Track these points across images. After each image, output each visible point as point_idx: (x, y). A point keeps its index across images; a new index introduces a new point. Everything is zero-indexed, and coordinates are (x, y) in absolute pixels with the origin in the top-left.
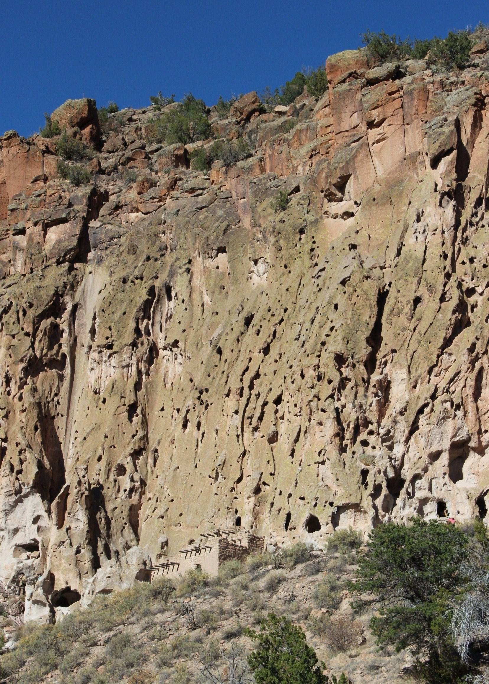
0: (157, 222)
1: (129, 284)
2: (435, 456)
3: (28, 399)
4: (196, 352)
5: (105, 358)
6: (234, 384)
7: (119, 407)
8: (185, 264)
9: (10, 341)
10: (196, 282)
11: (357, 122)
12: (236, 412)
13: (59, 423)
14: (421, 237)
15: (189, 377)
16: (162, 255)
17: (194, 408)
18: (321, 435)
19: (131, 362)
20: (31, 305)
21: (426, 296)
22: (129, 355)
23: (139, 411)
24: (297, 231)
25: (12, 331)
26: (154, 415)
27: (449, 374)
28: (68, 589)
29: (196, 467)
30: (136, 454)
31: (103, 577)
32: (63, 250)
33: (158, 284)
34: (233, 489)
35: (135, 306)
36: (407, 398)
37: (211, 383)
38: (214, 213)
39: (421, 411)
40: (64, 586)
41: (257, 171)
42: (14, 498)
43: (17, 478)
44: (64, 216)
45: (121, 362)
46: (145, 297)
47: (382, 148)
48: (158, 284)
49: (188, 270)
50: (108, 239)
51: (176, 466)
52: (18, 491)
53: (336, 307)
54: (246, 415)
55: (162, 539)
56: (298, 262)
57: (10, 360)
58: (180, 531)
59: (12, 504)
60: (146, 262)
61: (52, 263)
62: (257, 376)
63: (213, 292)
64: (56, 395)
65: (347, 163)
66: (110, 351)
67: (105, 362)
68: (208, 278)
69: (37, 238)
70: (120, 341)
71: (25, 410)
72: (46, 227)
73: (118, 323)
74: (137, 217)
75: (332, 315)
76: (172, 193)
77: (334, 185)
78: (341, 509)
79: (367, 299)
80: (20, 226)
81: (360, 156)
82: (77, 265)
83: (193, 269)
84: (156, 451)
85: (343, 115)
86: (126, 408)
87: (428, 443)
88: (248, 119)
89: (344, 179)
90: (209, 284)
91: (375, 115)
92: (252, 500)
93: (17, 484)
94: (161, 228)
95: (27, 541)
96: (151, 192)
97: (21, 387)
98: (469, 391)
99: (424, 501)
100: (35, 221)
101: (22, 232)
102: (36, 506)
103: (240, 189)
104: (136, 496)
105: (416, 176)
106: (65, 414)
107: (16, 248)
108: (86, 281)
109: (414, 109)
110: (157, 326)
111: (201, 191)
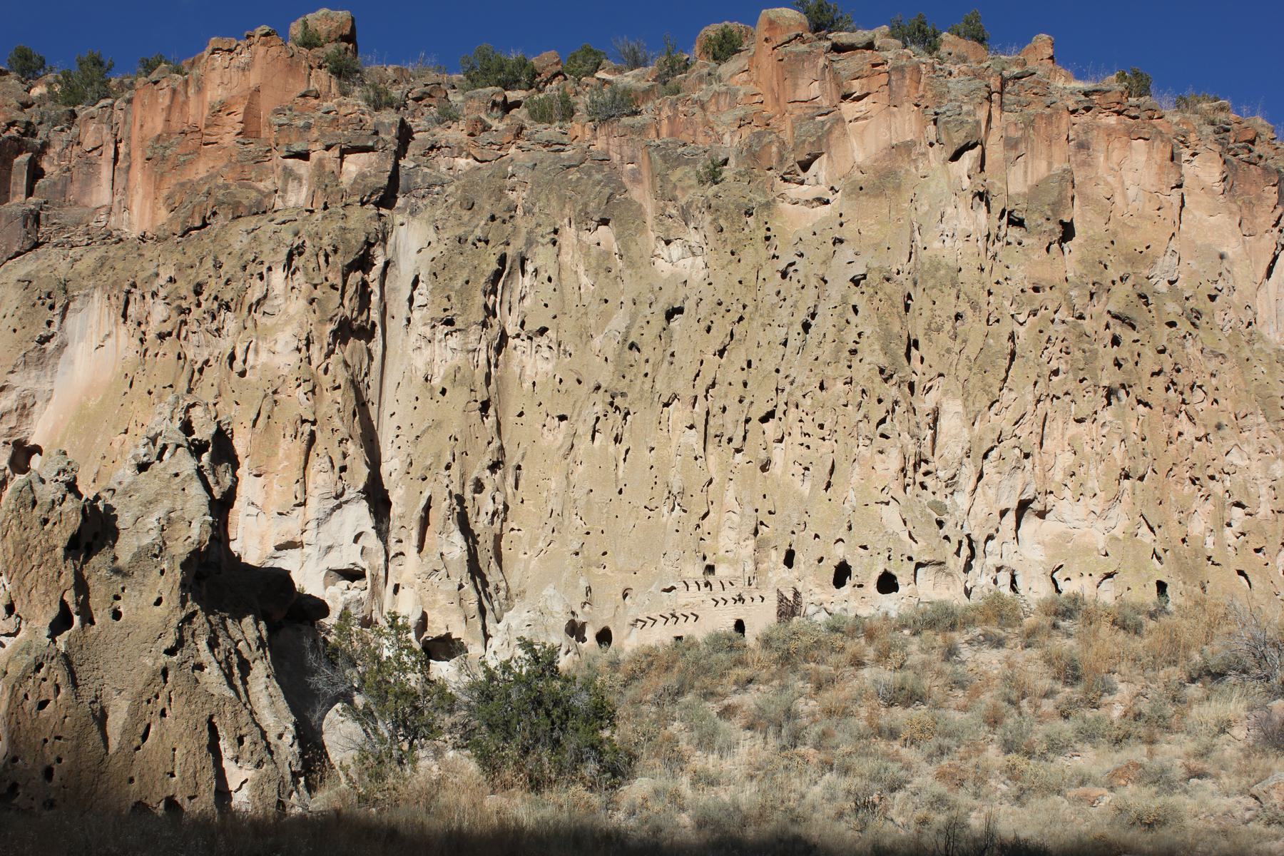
0: (501, 174)
1: (469, 245)
2: (1003, 513)
3: (342, 377)
4: (580, 346)
5: (439, 336)
6: (687, 394)
7: (469, 402)
8: (549, 234)
9: (311, 292)
10: (566, 258)
11: (818, 93)
12: (691, 427)
15: (576, 377)
16: (511, 217)
17: (605, 415)
18: (883, 466)
19: (479, 347)
21: (969, 313)
22: (478, 337)
23: (491, 411)
24: (743, 211)
25: (313, 279)
26: (510, 419)
27: (1011, 415)
28: (448, 635)
29: (620, 492)
31: (521, 624)
32: (370, 188)
33: (511, 252)
34: (698, 526)
35: (483, 275)
36: (966, 434)
37: (629, 387)
38: (590, 176)
39: (985, 456)
40: (443, 632)
41: (653, 133)
43: (340, 478)
44: (370, 143)
45: (466, 343)
46: (495, 266)
47: (865, 127)
48: (511, 252)
49: (554, 243)
50: (426, 185)
51: (589, 488)
53: (856, 310)
54: (711, 431)
55: (583, 583)
56: (749, 250)
57: (314, 318)
58: (604, 574)
59: (328, 511)
60: (490, 223)
61: (354, 202)
63: (597, 274)
64: (366, 375)
65: (819, 139)
66: (450, 328)
67: (440, 341)
68: (587, 255)
69: (332, 166)
70: (465, 316)
71: (339, 387)
72: (343, 153)
73: (460, 293)
74: (468, 164)
76: (518, 141)
77: (798, 162)
79: (893, 305)
80: (298, 147)
81: (836, 133)
82: (383, 211)
83: (560, 240)
84: (519, 468)
85: (800, 82)
86: (478, 405)
90: (589, 263)
91: (857, 87)
92: (751, 543)
93: (340, 486)
94: (509, 182)
95: (344, 565)
96: (485, 137)
97: (328, 356)
100: (329, 143)
101: (304, 156)
105: (914, 170)
106: (376, 402)
107: (288, 174)
108: (397, 233)
109: (905, 89)
110: (506, 307)
111: (562, 147)
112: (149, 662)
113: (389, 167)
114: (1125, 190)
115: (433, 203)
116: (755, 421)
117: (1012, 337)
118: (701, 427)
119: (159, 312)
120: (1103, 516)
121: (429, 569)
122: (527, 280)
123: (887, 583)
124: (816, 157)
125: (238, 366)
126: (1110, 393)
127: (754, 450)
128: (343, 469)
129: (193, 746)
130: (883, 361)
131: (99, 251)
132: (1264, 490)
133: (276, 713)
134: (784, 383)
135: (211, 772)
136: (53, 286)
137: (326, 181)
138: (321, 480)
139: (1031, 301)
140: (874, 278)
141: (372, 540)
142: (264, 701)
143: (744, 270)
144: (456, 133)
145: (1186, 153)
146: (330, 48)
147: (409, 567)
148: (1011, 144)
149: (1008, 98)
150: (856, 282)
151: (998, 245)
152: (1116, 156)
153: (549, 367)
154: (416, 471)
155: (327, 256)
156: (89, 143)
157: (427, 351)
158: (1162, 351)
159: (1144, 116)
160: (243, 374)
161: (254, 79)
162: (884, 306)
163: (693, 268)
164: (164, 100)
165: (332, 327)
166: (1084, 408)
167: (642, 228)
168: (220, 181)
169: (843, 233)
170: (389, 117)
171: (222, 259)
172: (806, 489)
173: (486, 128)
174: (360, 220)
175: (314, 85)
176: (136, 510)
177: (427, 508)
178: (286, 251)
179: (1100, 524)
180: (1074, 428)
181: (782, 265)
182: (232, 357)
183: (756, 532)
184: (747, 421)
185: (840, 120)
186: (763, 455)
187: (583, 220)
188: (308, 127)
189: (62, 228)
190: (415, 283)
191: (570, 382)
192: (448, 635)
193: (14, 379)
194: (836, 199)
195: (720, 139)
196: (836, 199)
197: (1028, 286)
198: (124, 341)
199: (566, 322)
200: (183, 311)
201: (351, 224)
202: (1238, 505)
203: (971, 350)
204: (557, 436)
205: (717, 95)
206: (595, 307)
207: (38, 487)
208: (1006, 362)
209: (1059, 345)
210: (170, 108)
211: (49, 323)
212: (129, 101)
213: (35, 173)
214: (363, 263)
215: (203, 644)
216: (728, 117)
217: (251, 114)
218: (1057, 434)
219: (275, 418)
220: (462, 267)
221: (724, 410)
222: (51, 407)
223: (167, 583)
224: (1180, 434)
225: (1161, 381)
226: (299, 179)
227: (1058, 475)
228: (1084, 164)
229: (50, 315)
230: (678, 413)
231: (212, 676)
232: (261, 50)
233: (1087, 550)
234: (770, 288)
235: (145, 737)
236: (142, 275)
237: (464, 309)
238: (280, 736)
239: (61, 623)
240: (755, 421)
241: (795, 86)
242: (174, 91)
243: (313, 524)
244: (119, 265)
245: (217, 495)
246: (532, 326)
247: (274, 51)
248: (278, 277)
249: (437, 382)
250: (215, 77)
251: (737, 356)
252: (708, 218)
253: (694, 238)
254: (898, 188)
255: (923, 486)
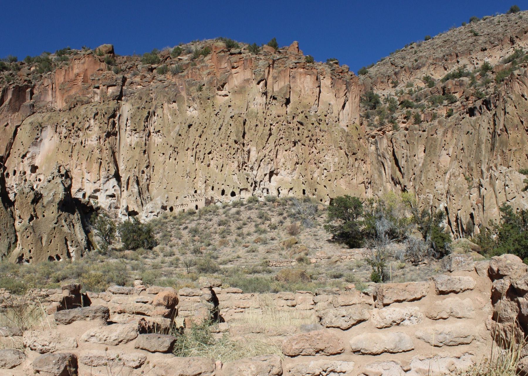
1: (140, 110)
2: (265, 175)
3: (108, 146)
5: (133, 134)
6: (191, 148)
10: (165, 111)
12: (192, 156)
13: (117, 155)
14: (256, 106)
20: (106, 113)
21: (259, 124)
23: (147, 153)
26: (152, 154)
27: (269, 150)
28: (134, 211)
30: (147, 167)
33: (151, 111)
36: (257, 156)
38: (171, 89)
39: (261, 161)
41: (187, 77)
42: (106, 179)
46: (147, 115)
48: (151, 111)
49: (162, 107)
52: (108, 177)
53: (230, 125)
55: (166, 196)
56: (208, 109)
57: (101, 132)
62: (198, 145)
68: (170, 110)
72: (108, 87)
73: (138, 122)
75: (230, 128)
78: (241, 190)
80: (97, 85)
81: (230, 77)
82: (119, 101)
83: (164, 107)
87: (264, 171)
88: (166, 59)
89: (225, 84)
91: (235, 65)
92: (204, 185)
94: (151, 92)
95: (110, 194)
96: (145, 80)
97: (105, 141)
98: (275, 156)
99: (263, 189)
102: (114, 182)
103: (180, 82)
104: (148, 181)
107: (95, 93)
112: (51, 226)
113: (120, 90)
114: (304, 88)
115: (132, 98)
116: (207, 154)
117: (270, 130)
118: (194, 156)
119: (64, 130)
120: (291, 174)
121: (129, 194)
122: (156, 118)
123: (233, 194)
124: (226, 83)
125: (83, 145)
126: (295, 143)
127: (206, 162)
128: (109, 170)
129: (62, 244)
130: (235, 138)
131: (49, 114)
132: (332, 165)
133: (81, 235)
134: (213, 144)
135: (66, 249)
136: (38, 124)
137: (104, 95)
138: (103, 173)
139: (277, 119)
140: (236, 116)
141: (117, 188)
142: (79, 232)
143: (207, 114)
144: (137, 79)
145: (322, 77)
146: (106, 56)
147: (125, 194)
148: (275, 78)
149: (275, 65)
150: (231, 117)
151: (269, 105)
152: (302, 80)
153: (161, 140)
154: (128, 169)
155: (104, 115)
156: (46, 84)
157: (130, 138)
158: (309, 131)
159: (310, 68)
160: (84, 147)
161: (86, 66)
162: (238, 124)
163: (195, 113)
164: (63, 73)
165: (105, 134)
166: (287, 147)
167: (184, 103)
168: (78, 95)
169: (231, 104)
170: (120, 76)
171: (79, 116)
172: (217, 171)
173: (145, 77)
174: (113, 104)
175: (102, 67)
176: (47, 192)
177: (129, 179)
178: (94, 114)
179: (290, 176)
180: (285, 152)
181: (216, 113)
182: (82, 143)
183: (206, 182)
184: (205, 154)
185: (231, 74)
186: (208, 163)
187: (169, 102)
188: (99, 80)
189: (40, 108)
190: (127, 120)
191: (165, 144)
192: (134, 211)
193: (30, 150)
194: (230, 95)
195: (203, 79)
196: (230, 95)
197: (276, 116)
198: (56, 137)
199: (165, 129)
200: (71, 131)
201: (110, 106)
202: (326, 169)
203: (259, 134)
204: (162, 159)
205: (203, 66)
206: (172, 124)
207: (24, 189)
208: (267, 137)
209: (283, 131)
210: (65, 75)
211: (38, 134)
212: (55, 73)
213: (32, 93)
214: (114, 116)
215: (63, 221)
216: (206, 72)
217: (85, 76)
218: (280, 154)
219: (92, 158)
220: (138, 116)
221: (200, 151)
222: (40, 156)
223: (54, 208)
224: (313, 152)
225: (308, 139)
226: (97, 94)
227: (281, 164)
228: (294, 82)
229: (37, 132)
230: (189, 152)
231: (66, 229)
232: (87, 59)
233: (286, 182)
234: (212, 119)
235: (51, 242)
236: (60, 121)
237: (139, 126)
238: (82, 240)
239: (31, 219)
240: (207, 154)
241: (221, 64)
242: (66, 70)
243: (102, 185)
244: (54, 118)
245: (66, 186)
246: (157, 130)
247: (90, 59)
248: (92, 121)
249: (133, 146)
250: (76, 66)
251: (204, 137)
252: (198, 101)
253: (195, 106)
254: (245, 91)
255: (245, 169)
